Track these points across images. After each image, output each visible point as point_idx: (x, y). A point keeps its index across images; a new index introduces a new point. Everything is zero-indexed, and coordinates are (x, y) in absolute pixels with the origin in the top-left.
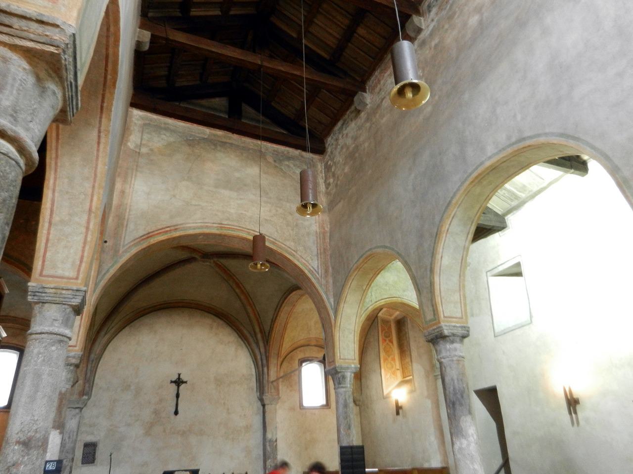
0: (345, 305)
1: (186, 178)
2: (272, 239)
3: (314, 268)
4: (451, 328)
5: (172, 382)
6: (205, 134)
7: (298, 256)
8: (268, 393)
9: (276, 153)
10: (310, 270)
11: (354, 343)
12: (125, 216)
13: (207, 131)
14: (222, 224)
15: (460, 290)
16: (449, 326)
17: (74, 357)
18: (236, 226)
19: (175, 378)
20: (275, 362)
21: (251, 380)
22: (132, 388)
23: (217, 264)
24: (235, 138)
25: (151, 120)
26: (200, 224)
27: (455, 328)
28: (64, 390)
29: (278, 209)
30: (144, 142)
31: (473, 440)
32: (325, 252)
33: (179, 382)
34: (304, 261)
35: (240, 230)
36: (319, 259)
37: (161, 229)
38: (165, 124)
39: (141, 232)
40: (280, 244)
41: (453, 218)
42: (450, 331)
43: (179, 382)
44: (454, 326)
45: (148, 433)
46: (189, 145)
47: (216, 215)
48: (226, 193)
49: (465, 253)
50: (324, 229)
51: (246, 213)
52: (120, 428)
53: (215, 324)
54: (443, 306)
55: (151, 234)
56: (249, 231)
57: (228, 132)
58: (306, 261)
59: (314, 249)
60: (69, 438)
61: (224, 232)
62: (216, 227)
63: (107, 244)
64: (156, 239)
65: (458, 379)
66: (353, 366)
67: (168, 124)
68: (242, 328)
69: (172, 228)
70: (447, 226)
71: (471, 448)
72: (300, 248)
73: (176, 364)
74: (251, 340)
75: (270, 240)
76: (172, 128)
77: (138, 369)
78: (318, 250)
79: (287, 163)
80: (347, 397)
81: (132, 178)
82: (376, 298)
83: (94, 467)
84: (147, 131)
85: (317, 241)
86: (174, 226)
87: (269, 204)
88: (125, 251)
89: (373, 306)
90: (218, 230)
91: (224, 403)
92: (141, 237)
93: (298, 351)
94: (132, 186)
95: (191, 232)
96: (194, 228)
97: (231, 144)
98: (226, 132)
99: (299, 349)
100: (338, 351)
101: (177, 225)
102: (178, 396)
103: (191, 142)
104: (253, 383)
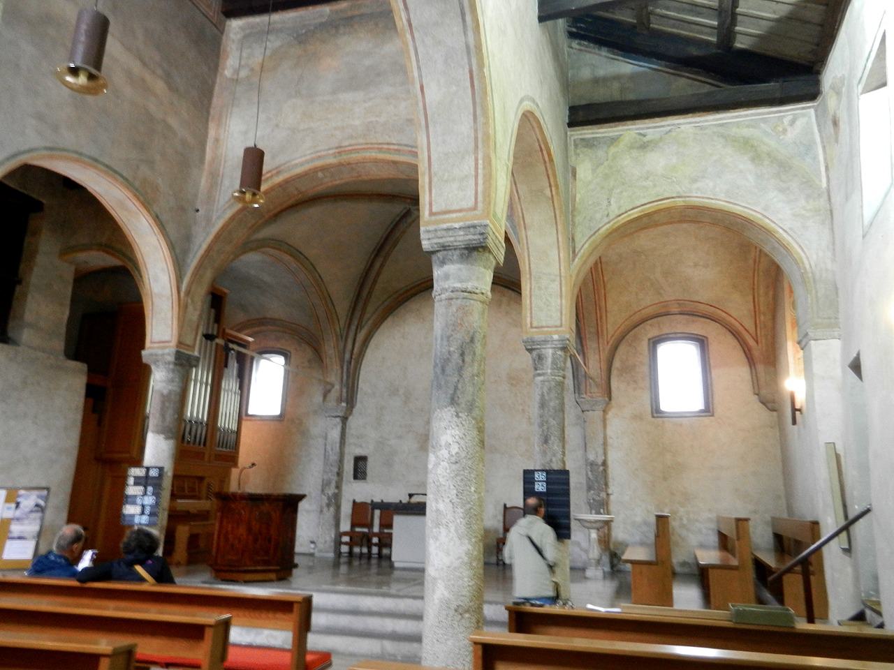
0: (529, 233)
4: (439, 234)
6: (322, 16)
8: (586, 393)
11: (561, 296)
14: (341, 147)
15: (476, 147)
16: (436, 230)
17: (169, 354)
20: (595, 345)
22: (402, 391)
26: (308, 157)
27: (450, 233)
28: (165, 392)
30: (243, 63)
31: (447, 455)
44: (448, 229)
48: (347, 97)
49: (474, 61)
51: (377, 119)
52: (389, 440)
53: (505, 300)
60: (332, 450)
61: (345, 158)
62: (332, 154)
63: (200, 213)
66: (556, 337)
71: (440, 471)
80: (545, 390)
82: (619, 208)
83: (365, 484)
88: (219, 218)
89: (612, 223)
90: (335, 157)
91: (523, 410)
93: (647, 325)
94: (227, 128)
95: (299, 170)
96: (302, 164)
97: (361, 16)
99: (649, 322)
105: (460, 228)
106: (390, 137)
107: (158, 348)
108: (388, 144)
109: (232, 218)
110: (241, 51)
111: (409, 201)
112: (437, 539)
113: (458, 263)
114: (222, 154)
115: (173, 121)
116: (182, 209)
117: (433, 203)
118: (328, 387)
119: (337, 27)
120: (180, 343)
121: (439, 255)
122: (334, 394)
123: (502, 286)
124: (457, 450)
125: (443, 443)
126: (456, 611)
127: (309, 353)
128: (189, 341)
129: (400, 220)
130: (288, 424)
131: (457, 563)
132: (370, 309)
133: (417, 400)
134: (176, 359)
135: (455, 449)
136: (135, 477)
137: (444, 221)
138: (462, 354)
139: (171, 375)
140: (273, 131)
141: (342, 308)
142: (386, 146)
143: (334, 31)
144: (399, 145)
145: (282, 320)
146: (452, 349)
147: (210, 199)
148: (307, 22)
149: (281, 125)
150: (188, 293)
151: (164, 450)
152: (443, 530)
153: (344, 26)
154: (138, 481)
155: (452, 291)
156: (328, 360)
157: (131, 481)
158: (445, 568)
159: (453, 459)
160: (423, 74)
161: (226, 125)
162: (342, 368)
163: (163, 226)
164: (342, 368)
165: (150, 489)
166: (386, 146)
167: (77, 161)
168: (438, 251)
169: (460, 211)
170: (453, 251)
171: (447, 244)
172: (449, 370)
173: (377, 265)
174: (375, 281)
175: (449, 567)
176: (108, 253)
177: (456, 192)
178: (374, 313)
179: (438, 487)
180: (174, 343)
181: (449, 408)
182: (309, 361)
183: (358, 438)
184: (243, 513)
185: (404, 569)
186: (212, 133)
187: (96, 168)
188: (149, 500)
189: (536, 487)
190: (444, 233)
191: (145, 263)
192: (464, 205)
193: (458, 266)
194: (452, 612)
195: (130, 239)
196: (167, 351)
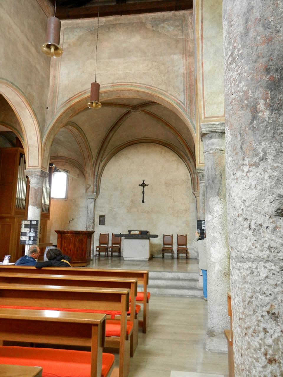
1: (90, 57)
2: (148, 86)
3: (180, 101)
5: (140, 185)
6: (102, 22)
7: (168, 95)
9: (154, 20)
10: (178, 104)
12: (56, 90)
13: (103, 20)
14: (113, 83)
18: (124, 82)
19: (141, 183)
21: (188, 183)
22: (119, 189)
23: (142, 110)
24: (123, 18)
25: (68, 25)
27: (214, 126)
28: (36, 188)
29: (153, 63)
30: (64, 41)
31: (217, 215)
32: (190, 87)
33: (143, 185)
34: (173, 98)
35: (126, 84)
36: (185, 93)
37: (77, 94)
38: (77, 24)
39: (66, 99)
40: (155, 88)
41: (202, 22)
42: (208, 129)
43: (143, 185)
44: (213, 124)
45: (129, 212)
46: (92, 34)
47: (110, 78)
48: (116, 60)
50: (190, 69)
51: (130, 71)
52: (114, 209)
53: (163, 151)
54: (205, 108)
55: (71, 99)
56: (132, 84)
57: (118, 16)
58: (175, 97)
59: (182, 87)
60: (90, 212)
61: (116, 88)
62: (110, 86)
63: (48, 109)
64: (74, 101)
65: (211, 169)
67: (79, 24)
68: (180, 151)
69: (83, 93)
70: (200, 32)
72: (170, 88)
73: (142, 175)
74: (186, 158)
75: (147, 87)
76: (81, 25)
77: (121, 179)
78: (184, 87)
79: (163, 25)
81: (59, 66)
83: (104, 227)
84: (66, 33)
85: (184, 80)
86: (84, 91)
87: (146, 61)
88: (58, 112)
90: (111, 87)
92: (66, 102)
97: (120, 24)
98: (116, 16)
100: (198, 158)
101: (85, 90)
102: (143, 193)
103: (93, 31)
104: (190, 185)
105: (219, 124)
106: (136, 80)
107: (32, 169)
108: (136, 83)
109: (64, 112)
110: (63, 36)
111: (131, 107)
112: (214, 247)
113: (217, 138)
114: (57, 83)
115: (38, 67)
116: (42, 107)
117: (206, 113)
118: (88, 186)
119: (109, 28)
120: (42, 167)
121: (209, 135)
122: (91, 189)
123: (163, 145)
124: (221, 213)
125: (215, 211)
126: (224, 274)
127: (78, 171)
128: (45, 166)
129: (124, 116)
130: (69, 202)
131: (224, 256)
132: (106, 153)
133: (126, 192)
134: (41, 174)
135: (220, 213)
136: (25, 224)
137: (213, 121)
138: (221, 175)
139: (38, 181)
140: (81, 74)
141: (95, 153)
142: (134, 84)
143: (108, 30)
144: (140, 84)
145: (66, 157)
146: (216, 173)
147: (53, 103)
148: (94, 25)
149: (85, 72)
150: (45, 145)
151: (37, 213)
152: (217, 244)
153: (112, 28)
154: (26, 226)
155: (216, 150)
156: (88, 175)
157: (23, 226)
158: (219, 259)
159: (220, 217)
160: (204, 58)
161: (58, 70)
162: (94, 178)
163: (36, 115)
164: (94, 178)
165: (32, 229)
166: (134, 84)
167: (6, 84)
168: (209, 133)
169: (218, 117)
170: (215, 134)
171: (213, 130)
172: (216, 181)
173: (111, 135)
174: (109, 141)
175: (251, 258)
176: (3, 125)
177: (216, 109)
178: (107, 155)
179: (213, 227)
180: (40, 167)
181: (217, 197)
182: (78, 175)
183: (101, 208)
184: (84, 240)
185: (129, 261)
186: (52, 74)
187: (12, 87)
188: (32, 234)
189: (202, 227)
190: (211, 126)
191: (25, 131)
192: (220, 114)
193: (217, 140)
194: (222, 275)
195: (19, 120)
196: (37, 170)
